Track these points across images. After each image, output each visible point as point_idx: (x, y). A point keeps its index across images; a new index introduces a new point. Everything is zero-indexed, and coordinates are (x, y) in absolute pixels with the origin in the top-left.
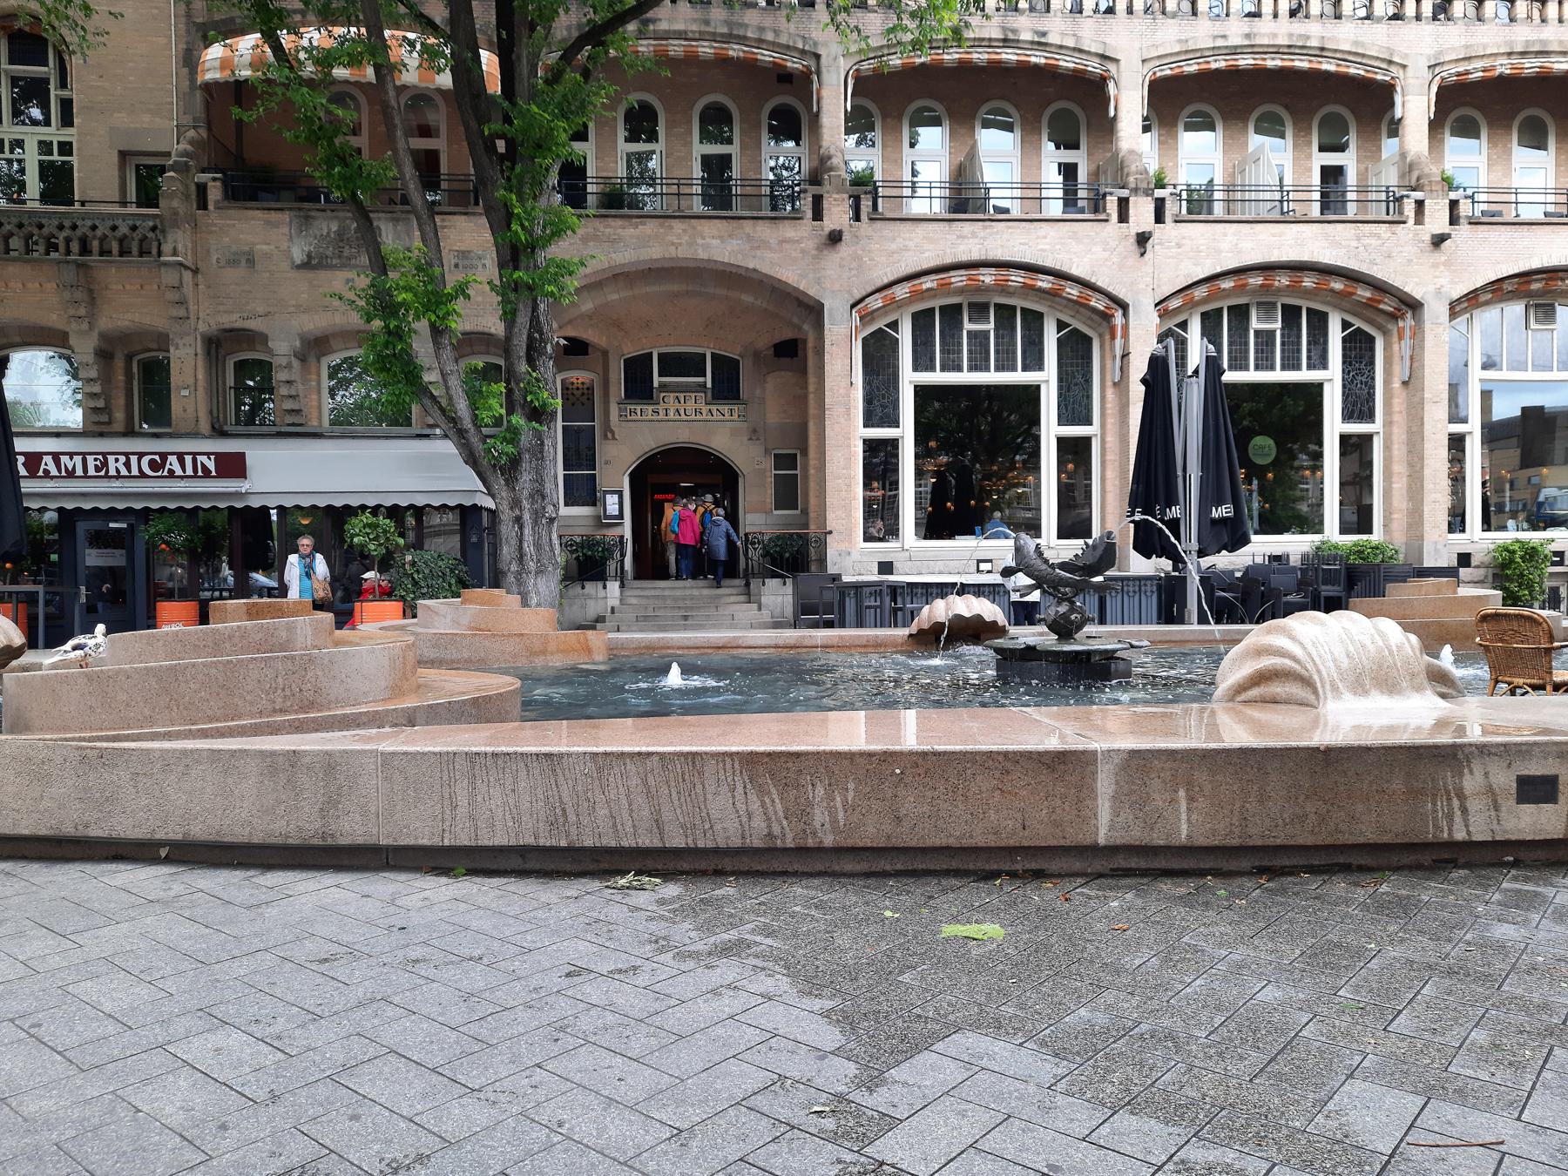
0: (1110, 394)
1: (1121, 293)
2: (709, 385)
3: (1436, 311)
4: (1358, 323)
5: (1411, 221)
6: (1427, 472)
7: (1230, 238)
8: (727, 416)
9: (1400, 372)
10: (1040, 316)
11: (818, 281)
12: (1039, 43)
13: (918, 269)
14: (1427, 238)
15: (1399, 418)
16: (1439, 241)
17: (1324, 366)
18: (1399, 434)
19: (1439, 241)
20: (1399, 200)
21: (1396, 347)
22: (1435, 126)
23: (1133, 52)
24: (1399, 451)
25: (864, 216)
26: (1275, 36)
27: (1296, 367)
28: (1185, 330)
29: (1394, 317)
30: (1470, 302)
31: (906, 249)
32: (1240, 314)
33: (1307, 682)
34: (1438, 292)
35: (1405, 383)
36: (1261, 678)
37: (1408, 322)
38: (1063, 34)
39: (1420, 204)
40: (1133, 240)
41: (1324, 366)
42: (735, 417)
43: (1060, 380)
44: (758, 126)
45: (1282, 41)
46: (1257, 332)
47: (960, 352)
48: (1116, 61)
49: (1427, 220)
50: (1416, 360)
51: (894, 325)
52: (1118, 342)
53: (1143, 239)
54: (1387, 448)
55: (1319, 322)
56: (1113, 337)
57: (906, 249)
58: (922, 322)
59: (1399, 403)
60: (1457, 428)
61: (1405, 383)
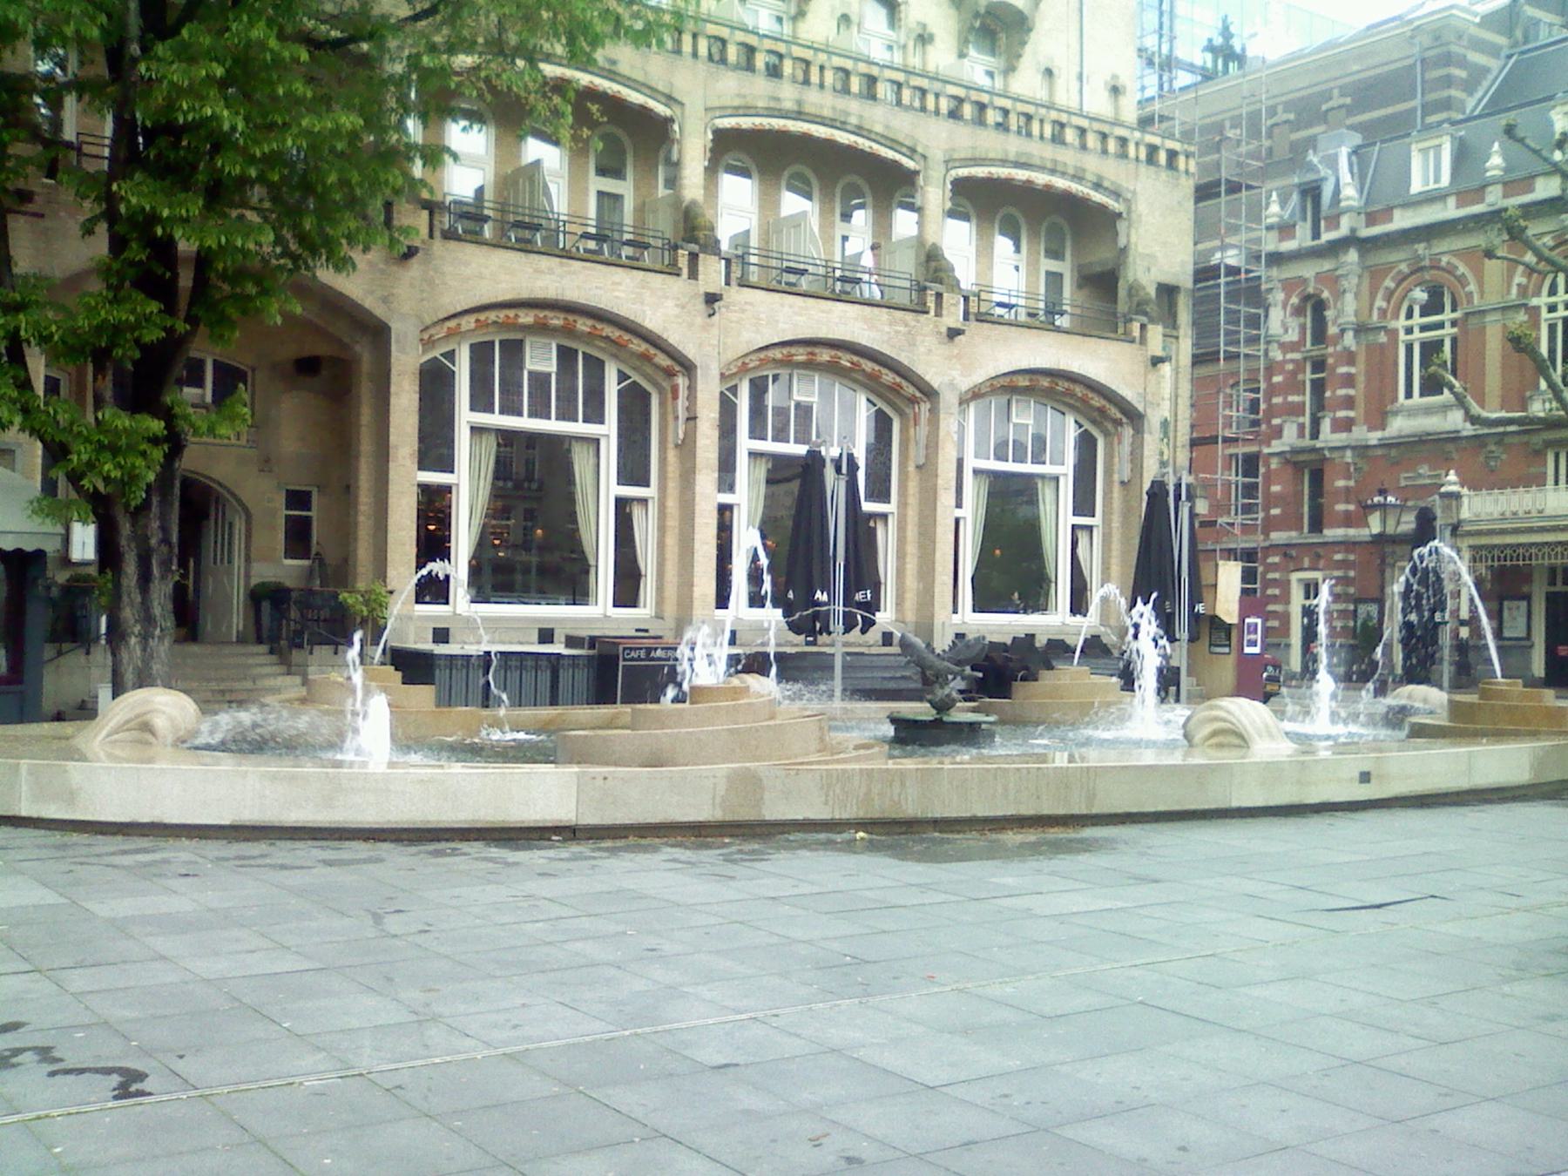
0: (672, 455)
1: (690, 351)
2: (209, 398)
3: (949, 400)
4: (635, 377)
5: (932, 313)
6: (938, 555)
7: (786, 309)
8: (233, 441)
9: (917, 455)
10: (601, 364)
11: (385, 300)
12: (610, 71)
13: (493, 300)
14: (944, 330)
15: (913, 500)
16: (953, 333)
17: (600, 420)
18: (912, 514)
19: (953, 333)
20: (925, 289)
21: (912, 431)
22: (712, 171)
23: (699, 99)
24: (912, 532)
25: (734, 283)
26: (822, 107)
27: (1023, 461)
28: (735, 395)
29: (913, 401)
30: (976, 394)
31: (481, 277)
32: (514, 350)
33: (1240, 736)
34: (952, 385)
35: (918, 467)
36: (1214, 734)
37: (925, 407)
38: (632, 67)
39: (939, 296)
40: (702, 299)
41: (600, 420)
42: (243, 442)
43: (620, 436)
44: (832, 210)
45: (827, 113)
46: (530, 373)
47: (521, 394)
48: (682, 104)
49: (944, 312)
50: (932, 446)
51: (450, 355)
52: (682, 403)
53: (712, 299)
54: (902, 528)
55: (595, 368)
56: (675, 397)
57: (481, 277)
58: (481, 354)
59: (913, 486)
60: (726, 498)
61: (918, 467)
